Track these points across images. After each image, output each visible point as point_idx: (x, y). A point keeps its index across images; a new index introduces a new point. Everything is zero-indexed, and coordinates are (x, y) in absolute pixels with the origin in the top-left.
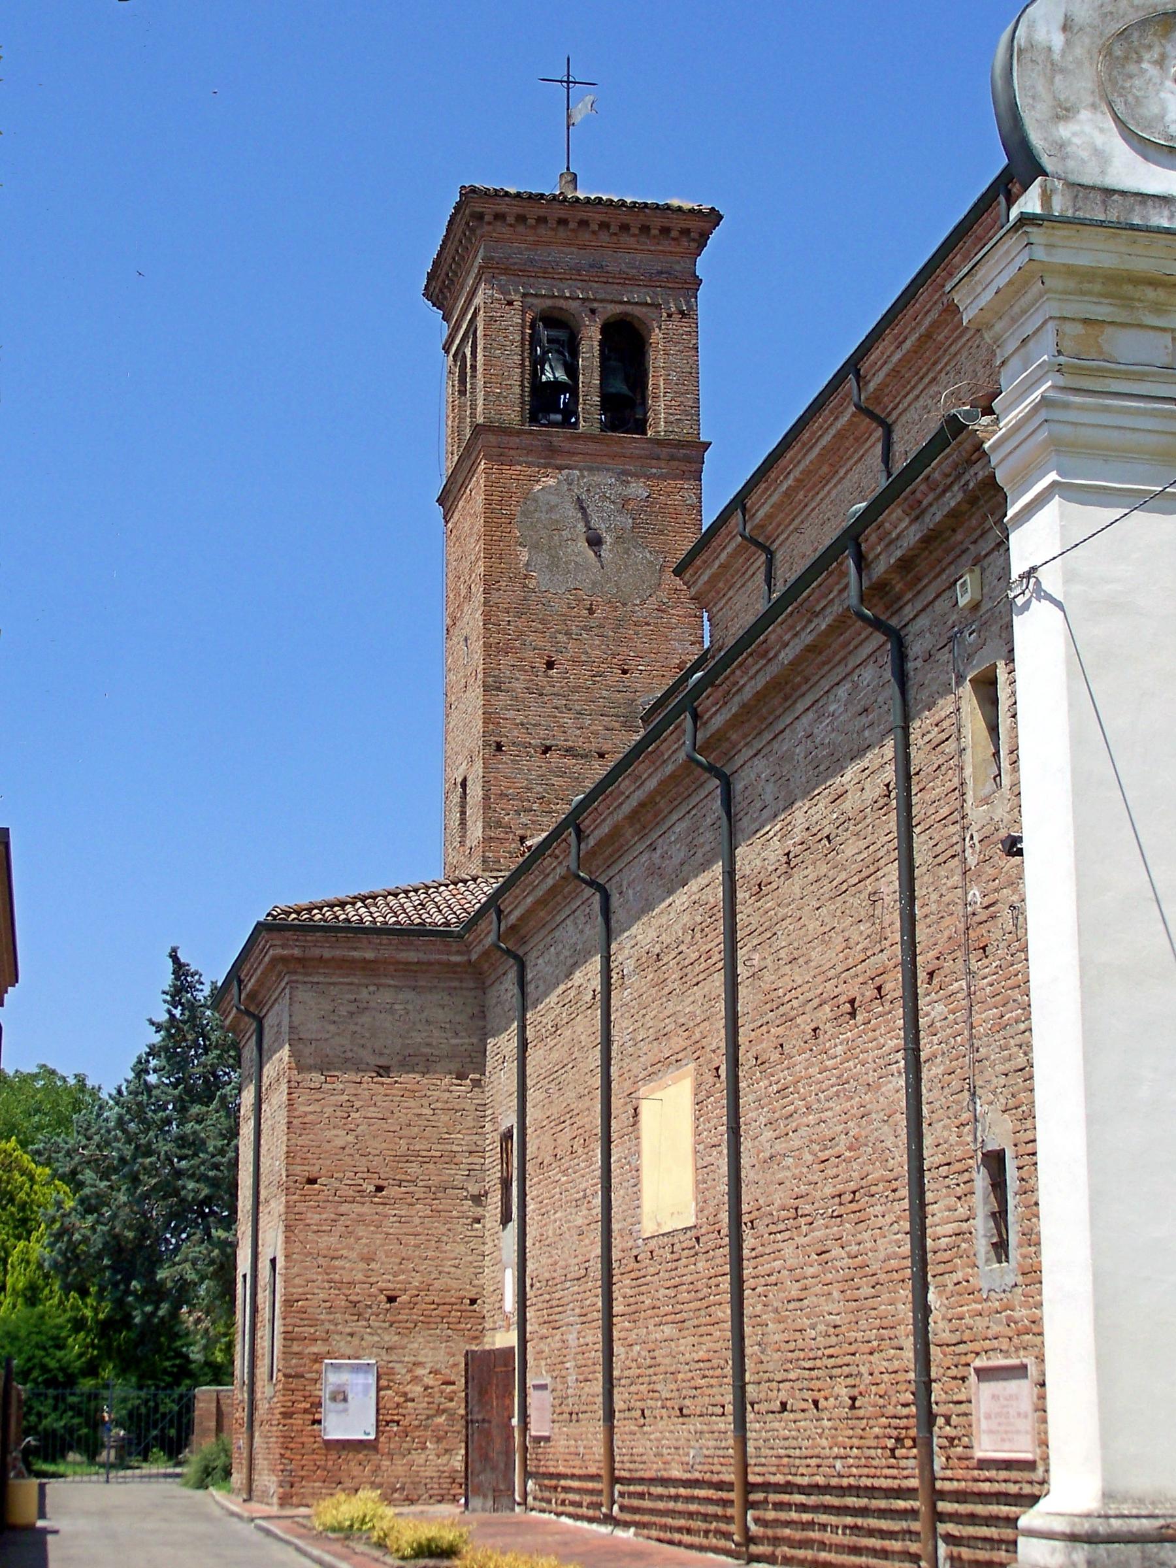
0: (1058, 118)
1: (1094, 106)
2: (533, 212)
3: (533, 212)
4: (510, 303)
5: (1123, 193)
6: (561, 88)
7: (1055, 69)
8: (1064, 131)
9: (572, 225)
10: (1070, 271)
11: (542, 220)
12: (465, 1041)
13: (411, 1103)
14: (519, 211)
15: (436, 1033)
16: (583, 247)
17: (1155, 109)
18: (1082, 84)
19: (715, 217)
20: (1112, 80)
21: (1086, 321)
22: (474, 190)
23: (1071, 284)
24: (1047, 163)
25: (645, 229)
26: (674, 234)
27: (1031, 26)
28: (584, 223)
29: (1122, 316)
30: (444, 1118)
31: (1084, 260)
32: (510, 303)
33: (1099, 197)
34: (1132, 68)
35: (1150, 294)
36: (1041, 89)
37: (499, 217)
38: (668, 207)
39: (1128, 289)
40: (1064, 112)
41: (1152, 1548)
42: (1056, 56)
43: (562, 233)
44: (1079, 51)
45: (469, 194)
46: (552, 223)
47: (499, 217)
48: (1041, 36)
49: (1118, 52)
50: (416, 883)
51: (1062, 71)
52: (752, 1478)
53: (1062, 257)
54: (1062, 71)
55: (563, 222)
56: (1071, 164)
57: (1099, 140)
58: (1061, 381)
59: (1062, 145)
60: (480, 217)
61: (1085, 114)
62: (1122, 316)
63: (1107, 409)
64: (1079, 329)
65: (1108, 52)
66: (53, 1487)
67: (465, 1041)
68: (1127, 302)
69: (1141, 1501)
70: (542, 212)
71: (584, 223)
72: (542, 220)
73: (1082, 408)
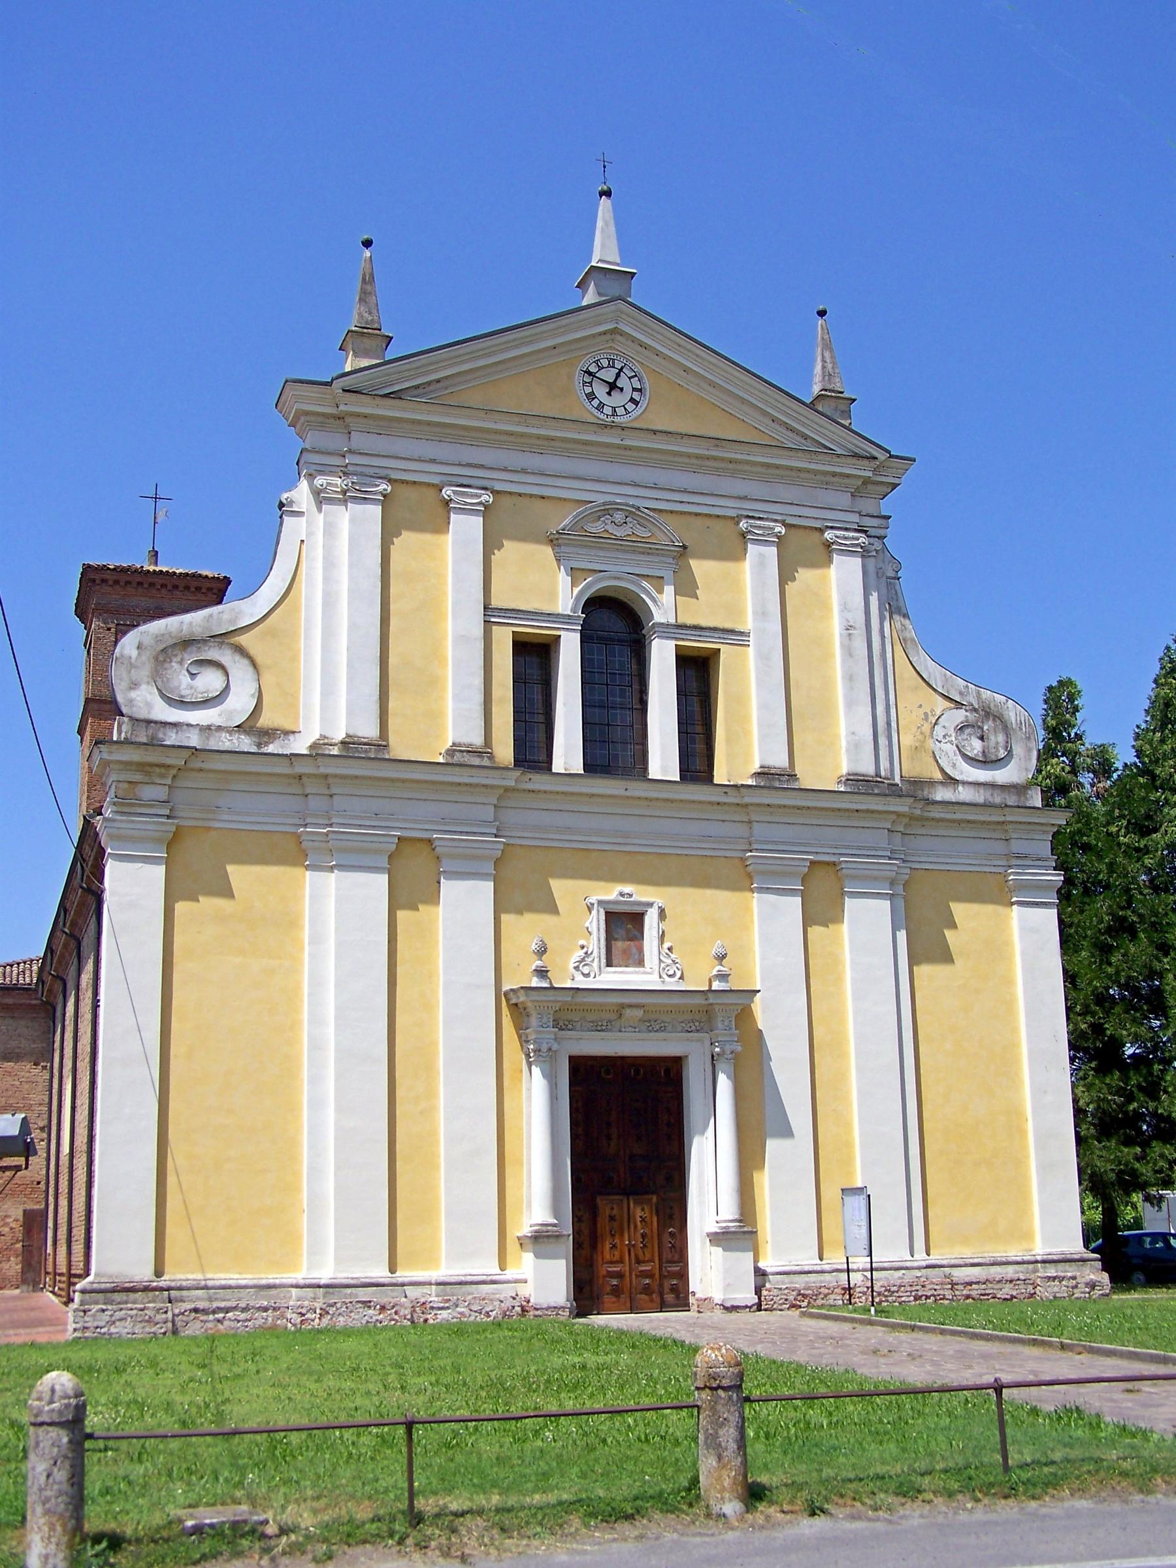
0: (131, 688)
1: (148, 683)
2: (123, 578)
3: (123, 578)
4: (109, 629)
5: (156, 722)
6: (159, 502)
7: (132, 666)
8: (133, 694)
9: (146, 586)
10: (121, 762)
11: (128, 583)
12: (38, 1046)
13: (9, 1079)
14: (115, 577)
15: (23, 1041)
16: (151, 597)
17: (176, 684)
18: (145, 673)
19: (227, 581)
20: (157, 671)
21: (129, 782)
22: (89, 566)
23: (122, 767)
24: (124, 710)
25: (187, 588)
26: (204, 590)
27: (123, 648)
28: (152, 585)
29: (146, 779)
30: (26, 1086)
31: (125, 758)
32: (109, 629)
33: (144, 725)
34: (167, 665)
35: (158, 770)
36: (124, 675)
37: (104, 581)
38: (200, 575)
39: (148, 769)
40: (134, 685)
41: (109, 1295)
42: (133, 661)
43: (140, 590)
44: (144, 658)
45: (87, 569)
46: (134, 585)
47: (104, 581)
48: (127, 652)
49: (161, 659)
50: (25, 958)
51: (136, 667)
52: (73, 1272)
53: (114, 757)
54: (136, 667)
55: (140, 584)
56: (135, 709)
57: (149, 698)
58: (115, 808)
59: (131, 701)
60: (94, 581)
61: (144, 687)
62: (146, 779)
63: (133, 822)
64: (126, 785)
65: (156, 658)
66: (886, 904)
67: (38, 1046)
68: (148, 774)
69: (111, 1277)
70: (128, 579)
71: (152, 585)
72: (128, 583)
73: (121, 821)
